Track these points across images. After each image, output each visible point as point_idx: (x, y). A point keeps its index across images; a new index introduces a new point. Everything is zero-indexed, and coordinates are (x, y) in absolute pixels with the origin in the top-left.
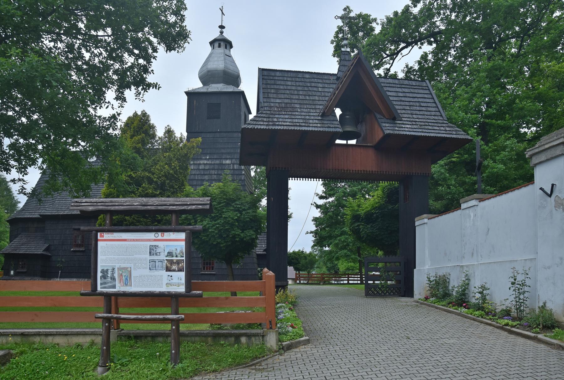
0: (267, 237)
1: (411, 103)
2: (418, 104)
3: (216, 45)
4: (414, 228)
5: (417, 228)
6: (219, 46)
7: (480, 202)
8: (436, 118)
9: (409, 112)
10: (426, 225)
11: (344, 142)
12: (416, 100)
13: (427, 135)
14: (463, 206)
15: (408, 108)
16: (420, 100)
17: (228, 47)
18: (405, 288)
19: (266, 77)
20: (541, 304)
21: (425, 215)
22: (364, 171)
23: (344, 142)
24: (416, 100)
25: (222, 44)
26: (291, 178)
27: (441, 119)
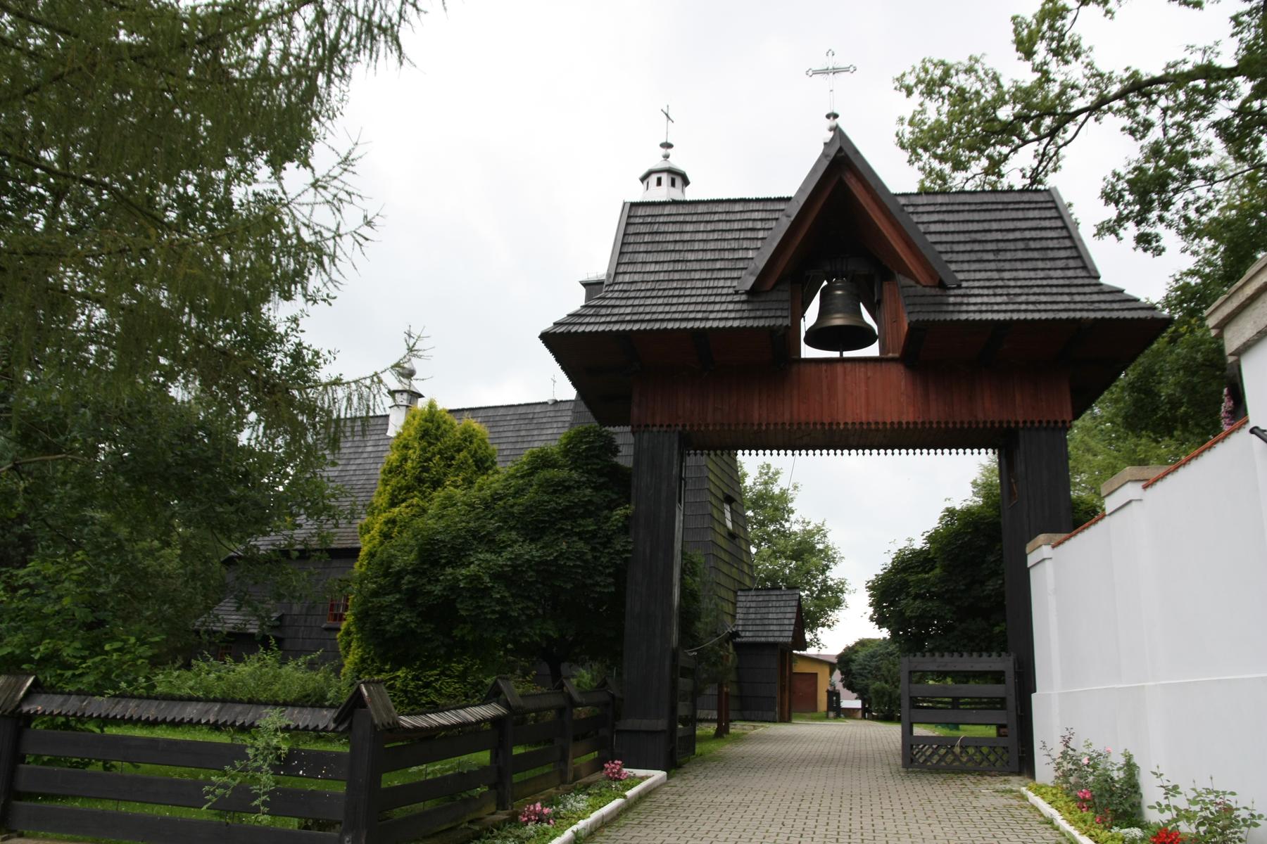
0: (796, 625)
1: (1001, 246)
2: (1021, 245)
3: (654, 178)
4: (1026, 572)
5: (1032, 572)
6: (659, 182)
7: (1145, 487)
8: (1070, 273)
9: (992, 266)
10: (1047, 562)
11: (836, 354)
12: (1018, 235)
13: (1107, 315)
14: (1110, 504)
15: (991, 256)
16: (1028, 234)
17: (678, 181)
18: (1024, 765)
19: (1050, 205)
20: (1121, 761)
21: (1042, 537)
22: (877, 423)
23: (836, 354)
24: (1018, 235)
25: (665, 177)
26: (740, 452)
27: (1083, 274)
